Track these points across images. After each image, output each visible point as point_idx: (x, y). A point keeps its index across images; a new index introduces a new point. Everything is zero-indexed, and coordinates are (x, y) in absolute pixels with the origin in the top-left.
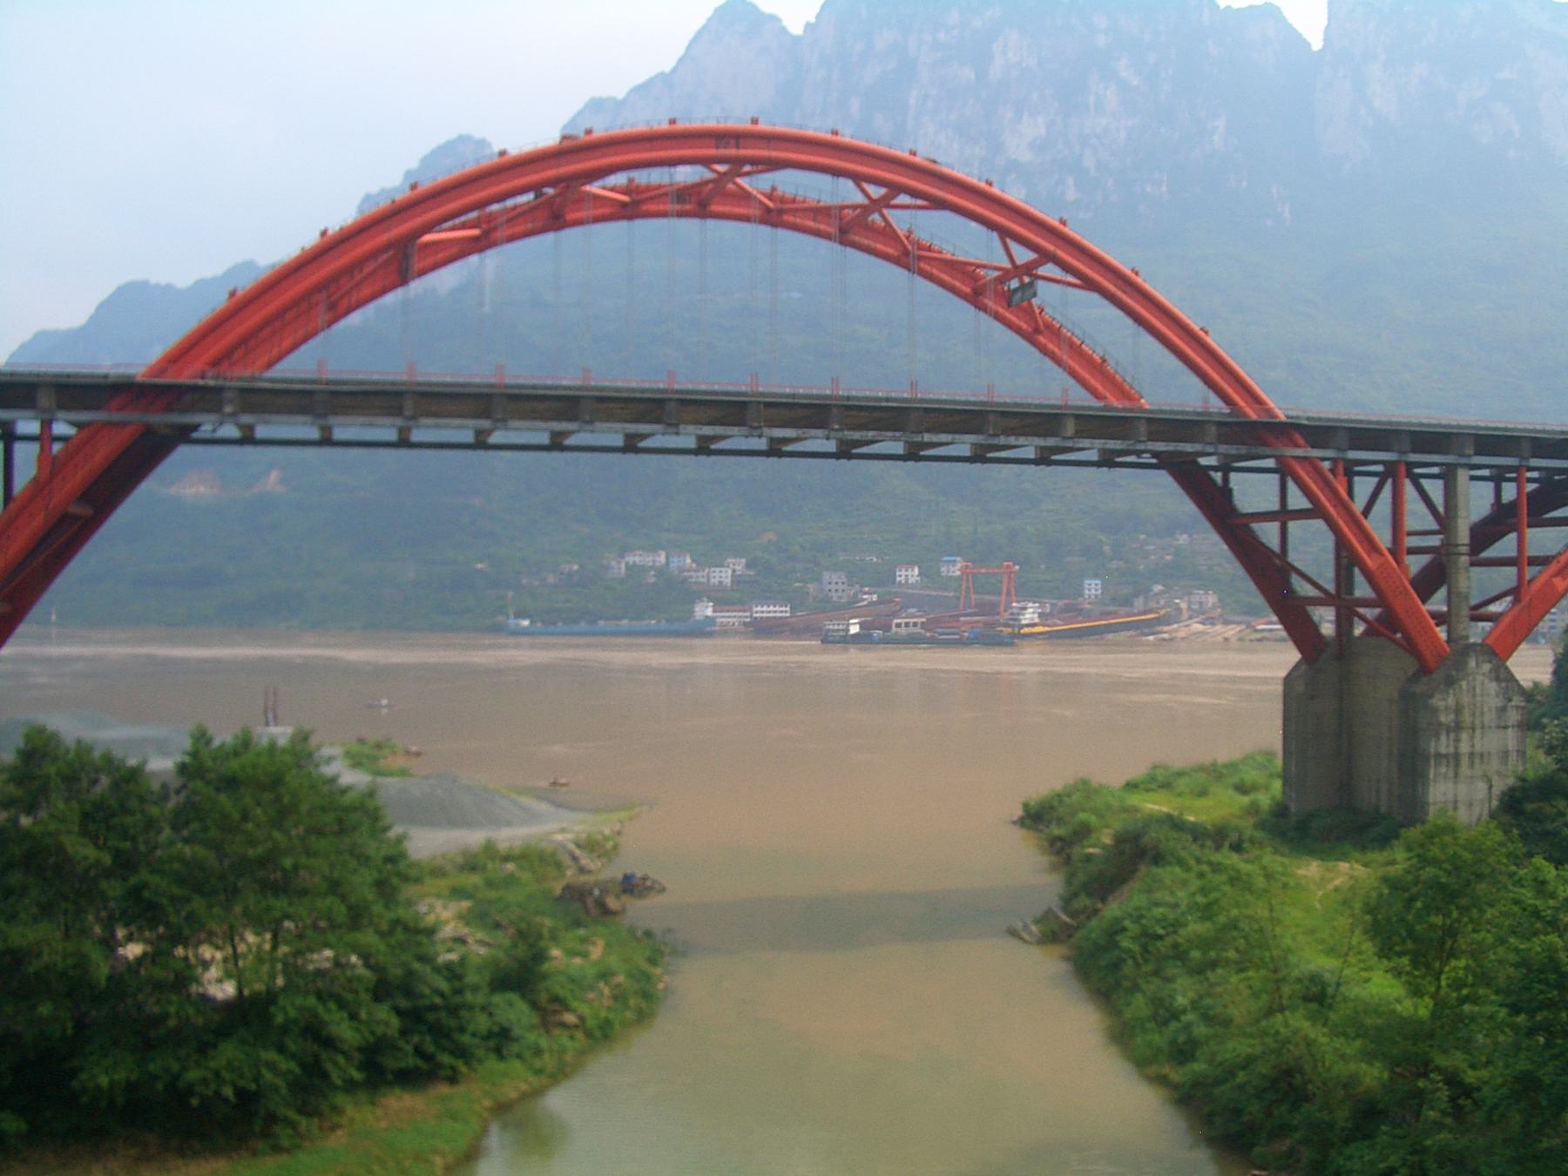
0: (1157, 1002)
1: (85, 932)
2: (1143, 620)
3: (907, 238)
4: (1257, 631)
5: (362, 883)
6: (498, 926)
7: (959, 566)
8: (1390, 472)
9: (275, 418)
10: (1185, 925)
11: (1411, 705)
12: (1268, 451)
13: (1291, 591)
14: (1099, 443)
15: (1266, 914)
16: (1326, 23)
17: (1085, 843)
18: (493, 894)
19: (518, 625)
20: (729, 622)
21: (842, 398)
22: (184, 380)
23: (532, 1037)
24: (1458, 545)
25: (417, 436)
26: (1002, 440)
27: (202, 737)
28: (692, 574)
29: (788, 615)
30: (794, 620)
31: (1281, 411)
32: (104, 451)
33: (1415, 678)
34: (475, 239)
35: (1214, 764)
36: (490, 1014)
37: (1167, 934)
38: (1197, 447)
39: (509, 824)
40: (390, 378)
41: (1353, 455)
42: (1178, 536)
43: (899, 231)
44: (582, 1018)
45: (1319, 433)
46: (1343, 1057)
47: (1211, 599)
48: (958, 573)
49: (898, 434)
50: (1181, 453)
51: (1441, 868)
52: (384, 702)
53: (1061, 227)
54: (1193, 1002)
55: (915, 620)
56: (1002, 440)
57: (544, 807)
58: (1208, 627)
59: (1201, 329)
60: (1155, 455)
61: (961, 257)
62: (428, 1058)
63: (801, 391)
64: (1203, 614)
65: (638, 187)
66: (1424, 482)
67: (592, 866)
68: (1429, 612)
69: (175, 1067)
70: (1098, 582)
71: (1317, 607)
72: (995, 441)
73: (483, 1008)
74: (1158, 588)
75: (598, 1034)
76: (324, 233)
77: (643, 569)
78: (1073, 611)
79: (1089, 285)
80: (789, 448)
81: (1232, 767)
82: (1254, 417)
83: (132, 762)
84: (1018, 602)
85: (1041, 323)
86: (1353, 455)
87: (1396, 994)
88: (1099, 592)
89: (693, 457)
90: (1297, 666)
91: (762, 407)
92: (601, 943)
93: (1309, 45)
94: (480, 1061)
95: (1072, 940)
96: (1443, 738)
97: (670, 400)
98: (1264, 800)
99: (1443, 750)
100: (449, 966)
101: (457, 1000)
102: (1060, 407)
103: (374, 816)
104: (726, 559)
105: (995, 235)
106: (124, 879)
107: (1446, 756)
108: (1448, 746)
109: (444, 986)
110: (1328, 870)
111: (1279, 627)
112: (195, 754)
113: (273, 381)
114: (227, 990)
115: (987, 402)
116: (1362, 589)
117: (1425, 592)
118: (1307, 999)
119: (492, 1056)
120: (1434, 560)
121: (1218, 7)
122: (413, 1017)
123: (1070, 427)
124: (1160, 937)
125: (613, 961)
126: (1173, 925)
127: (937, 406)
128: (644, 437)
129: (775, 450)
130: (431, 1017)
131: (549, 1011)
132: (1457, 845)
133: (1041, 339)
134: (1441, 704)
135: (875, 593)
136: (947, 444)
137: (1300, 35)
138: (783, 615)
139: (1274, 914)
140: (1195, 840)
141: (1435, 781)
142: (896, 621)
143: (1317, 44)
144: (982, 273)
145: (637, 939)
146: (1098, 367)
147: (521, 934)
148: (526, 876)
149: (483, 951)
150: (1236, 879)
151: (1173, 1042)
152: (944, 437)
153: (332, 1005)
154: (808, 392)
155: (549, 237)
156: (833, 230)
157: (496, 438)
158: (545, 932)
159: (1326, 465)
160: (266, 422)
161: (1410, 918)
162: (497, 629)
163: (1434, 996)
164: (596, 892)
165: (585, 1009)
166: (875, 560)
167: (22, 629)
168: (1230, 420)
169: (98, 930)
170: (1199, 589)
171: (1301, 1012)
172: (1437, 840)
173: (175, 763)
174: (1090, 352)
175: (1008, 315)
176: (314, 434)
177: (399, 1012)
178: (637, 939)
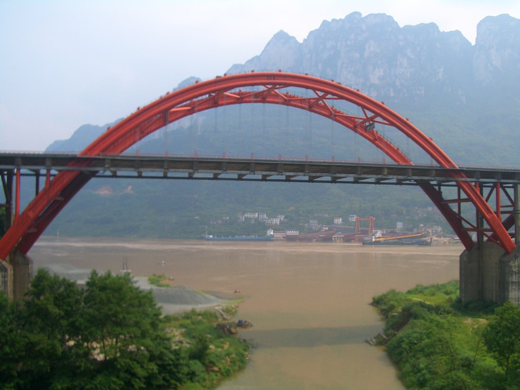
0: (414, 366)
1: (55, 338)
2: (417, 236)
3: (332, 109)
4: (455, 240)
5: (146, 323)
6: (194, 337)
7: (355, 218)
8: (495, 186)
9: (123, 169)
10: (424, 340)
11: (503, 265)
12: (453, 179)
13: (461, 226)
14: (395, 177)
15: (449, 336)
16: (476, 36)
17: (393, 311)
18: (194, 327)
19: (209, 237)
20: (278, 237)
21: (309, 162)
22: (93, 156)
23: (202, 375)
24: (518, 210)
25: (169, 175)
26: (363, 176)
27: (94, 273)
28: (267, 221)
29: (298, 234)
30: (300, 236)
31: (458, 164)
32: (66, 180)
33: (504, 255)
34: (189, 110)
35: (438, 285)
36: (189, 367)
37: (418, 343)
38: (429, 178)
39: (201, 303)
40: (160, 156)
41: (482, 180)
42: (429, 208)
43: (329, 107)
44: (220, 369)
45: (470, 173)
46: (475, 386)
47: (440, 229)
48: (355, 220)
49: (328, 174)
50: (424, 180)
51: (508, 322)
52: (163, 262)
53: (382, 105)
54: (426, 366)
55: (340, 236)
56: (363, 176)
57: (213, 298)
58: (438, 238)
59: (430, 138)
60: (415, 180)
61: (350, 115)
62: (167, 381)
63: (296, 160)
64: (437, 234)
65: (242, 93)
66: (506, 189)
67: (227, 318)
68: (509, 233)
69: (83, 384)
70: (402, 223)
71: (471, 232)
72: (361, 176)
73: (186, 365)
74: (422, 225)
75: (225, 374)
76: (138, 109)
77: (251, 219)
78: (393, 233)
79: (392, 124)
80: (268, 178)
81: (444, 286)
82: (448, 167)
83: (72, 281)
84: (374, 230)
85: (377, 137)
86: (482, 180)
87: (495, 365)
88: (402, 227)
89: (237, 181)
90: (464, 251)
91: (282, 165)
92: (228, 343)
93: (470, 44)
94: (185, 383)
95: (387, 345)
96: (514, 276)
97: (252, 163)
98: (454, 297)
99: (514, 280)
100: (175, 351)
101: (177, 362)
102: (382, 165)
103: (151, 300)
104: (278, 216)
105: (360, 108)
106: (68, 320)
107: (515, 282)
108: (516, 279)
109: (173, 357)
110: (474, 321)
111: (458, 238)
112: (92, 278)
113: (121, 157)
114: (101, 357)
115: (358, 163)
116: (486, 226)
117: (508, 227)
118: (463, 366)
119: (189, 381)
120: (511, 215)
121: (440, 31)
122: (163, 367)
123: (386, 172)
124: (415, 344)
125: (232, 350)
126: (419, 340)
127: (345, 165)
128: (244, 175)
129: (288, 179)
130: (169, 368)
131: (209, 366)
132: (514, 314)
133: (377, 142)
134: (513, 264)
135: (327, 227)
136: (345, 177)
137: (468, 40)
138: (297, 234)
139: (452, 337)
140: (429, 310)
141: (511, 291)
142: (334, 236)
143: (473, 43)
144: (357, 120)
145: (240, 342)
146: (396, 152)
147: (200, 340)
148: (205, 321)
149: (188, 346)
150: (439, 325)
151: (419, 380)
152: (343, 175)
153: (135, 363)
154: (298, 160)
155: (213, 110)
156: (307, 106)
157: (196, 175)
158: (208, 339)
159: (473, 184)
160: (120, 170)
161: (497, 339)
162: (202, 238)
163: (506, 366)
164: (228, 326)
165: (221, 366)
166: (327, 216)
167: (41, 237)
168: (439, 169)
169: (59, 336)
170: (436, 226)
171: (461, 371)
172: (507, 312)
173: (85, 282)
174: (393, 146)
175: (366, 134)
176: (136, 174)
177: (158, 365)
178: (240, 342)
